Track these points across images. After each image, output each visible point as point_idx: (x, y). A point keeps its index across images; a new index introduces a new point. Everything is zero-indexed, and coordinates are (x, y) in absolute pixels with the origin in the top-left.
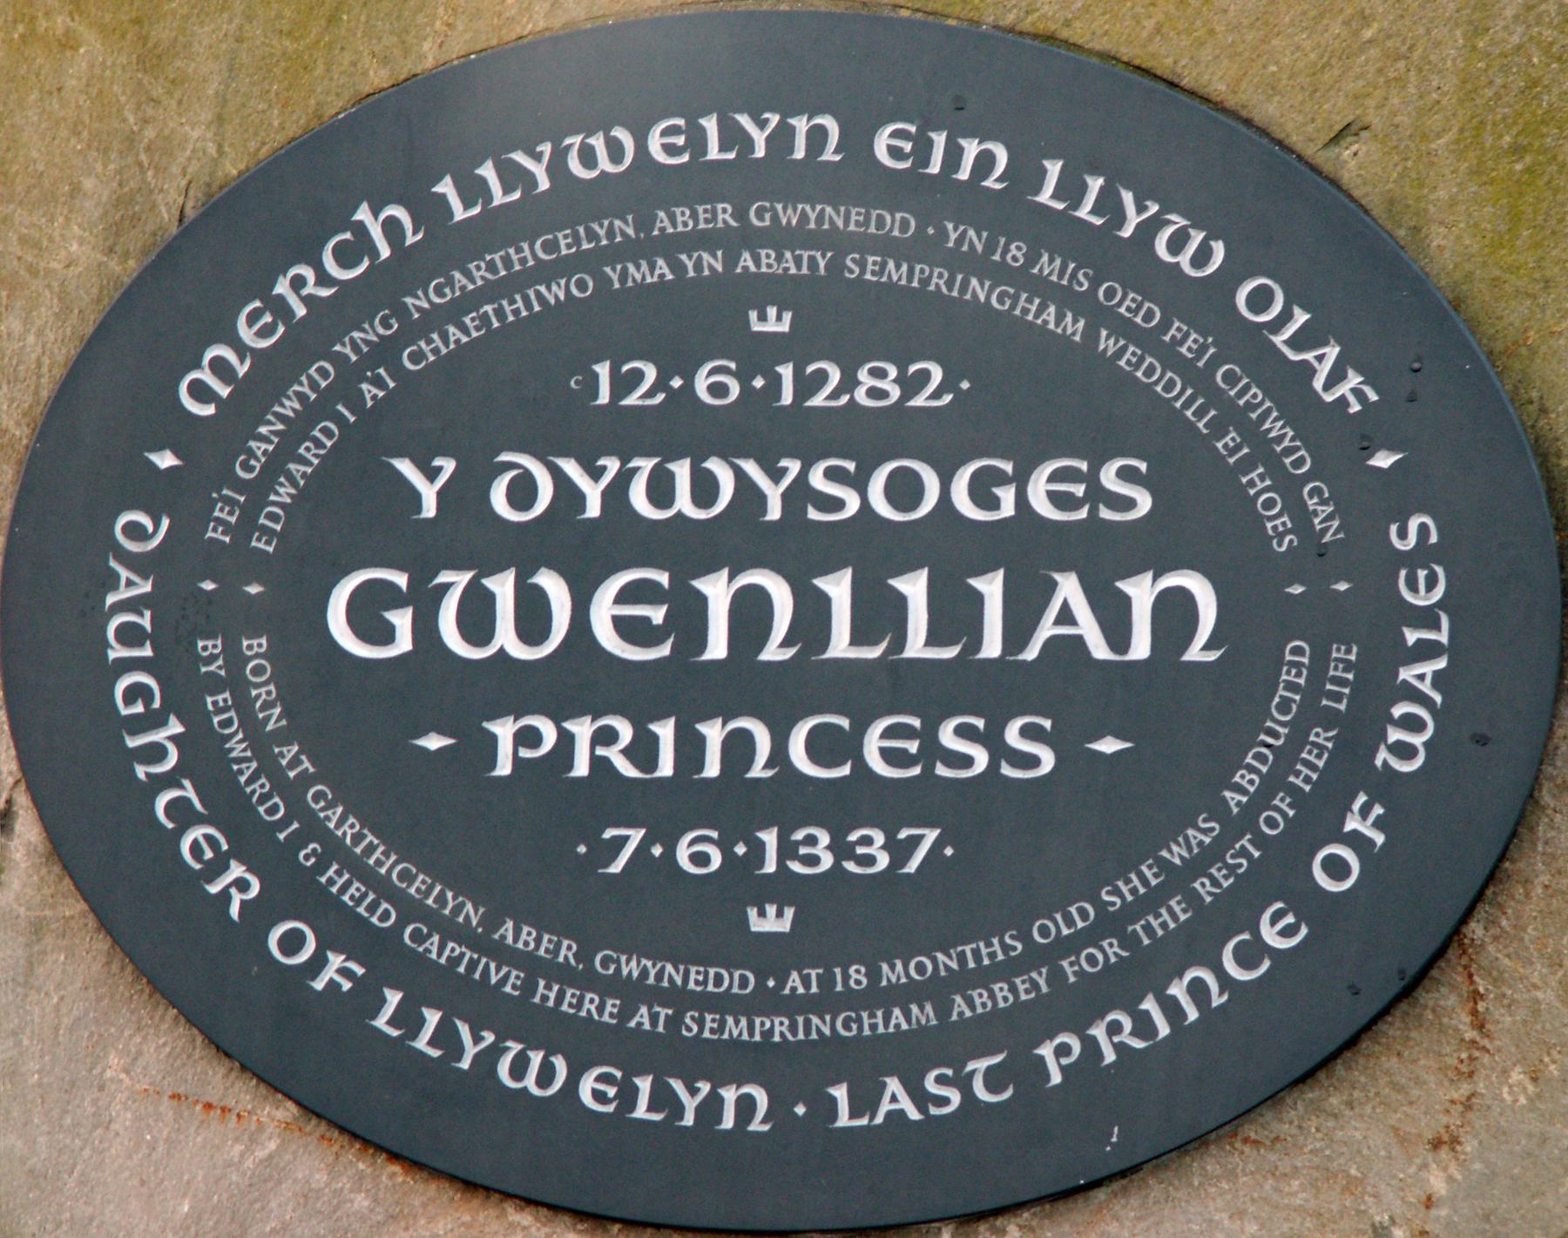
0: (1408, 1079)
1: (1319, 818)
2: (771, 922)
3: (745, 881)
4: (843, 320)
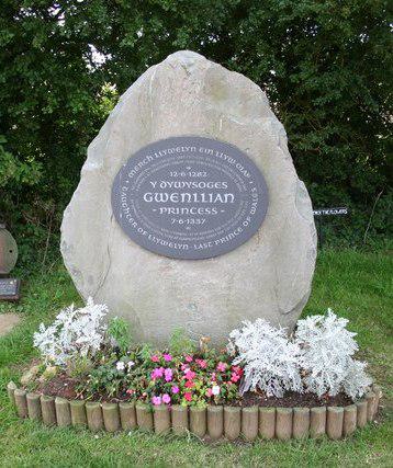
1: (244, 219)
4: (196, 168)
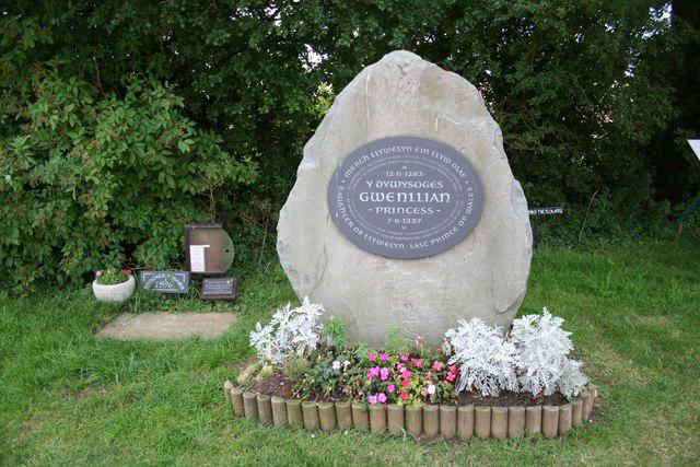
0: (468, 244)
1: (460, 218)
2: (404, 228)
3: (401, 224)
4: (412, 168)
